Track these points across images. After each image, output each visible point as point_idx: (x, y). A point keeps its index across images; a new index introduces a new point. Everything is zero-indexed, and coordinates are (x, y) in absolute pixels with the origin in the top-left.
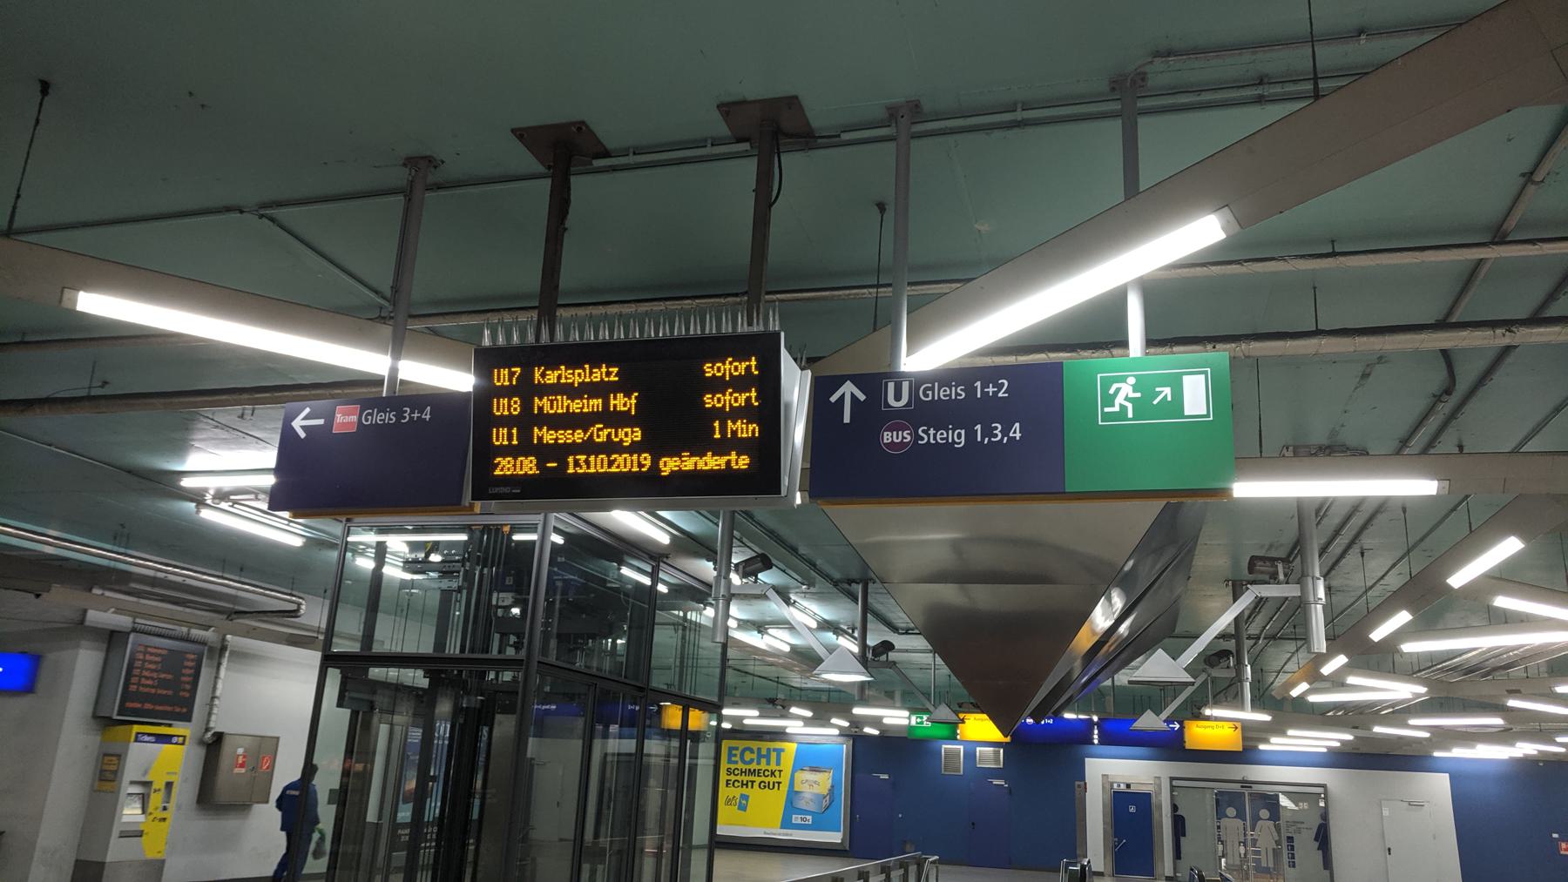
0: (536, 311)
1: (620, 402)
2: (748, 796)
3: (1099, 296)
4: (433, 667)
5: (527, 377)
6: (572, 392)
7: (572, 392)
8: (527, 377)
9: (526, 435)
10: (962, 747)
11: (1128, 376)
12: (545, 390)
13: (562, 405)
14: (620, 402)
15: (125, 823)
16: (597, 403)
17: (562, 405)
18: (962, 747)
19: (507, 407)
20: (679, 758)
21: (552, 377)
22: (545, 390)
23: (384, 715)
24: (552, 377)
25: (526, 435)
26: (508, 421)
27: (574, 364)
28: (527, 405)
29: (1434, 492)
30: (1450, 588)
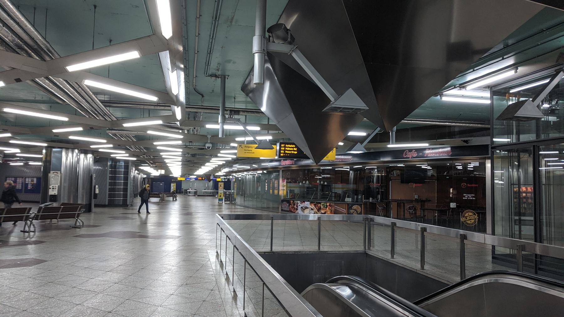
0: (507, 155)
1: (295, 149)
2: (533, 102)
3: (132, 90)
4: (27, 210)
5: (285, 146)
6: (290, 148)
7: (290, 148)
8: (285, 146)
9: (285, 152)
10: (490, 156)
11: (281, 160)
12: (287, 147)
13: (289, 149)
14: (295, 149)
15: (13, 221)
16: (292, 149)
17: (289, 149)
18: (490, 156)
19: (283, 149)
20: (400, 200)
21: (288, 146)
22: (287, 147)
23: (288, 184)
24: (288, 146)
25: (285, 152)
26: (283, 150)
27: (290, 145)
28: (285, 149)
29: (365, 135)
30: (66, 71)
